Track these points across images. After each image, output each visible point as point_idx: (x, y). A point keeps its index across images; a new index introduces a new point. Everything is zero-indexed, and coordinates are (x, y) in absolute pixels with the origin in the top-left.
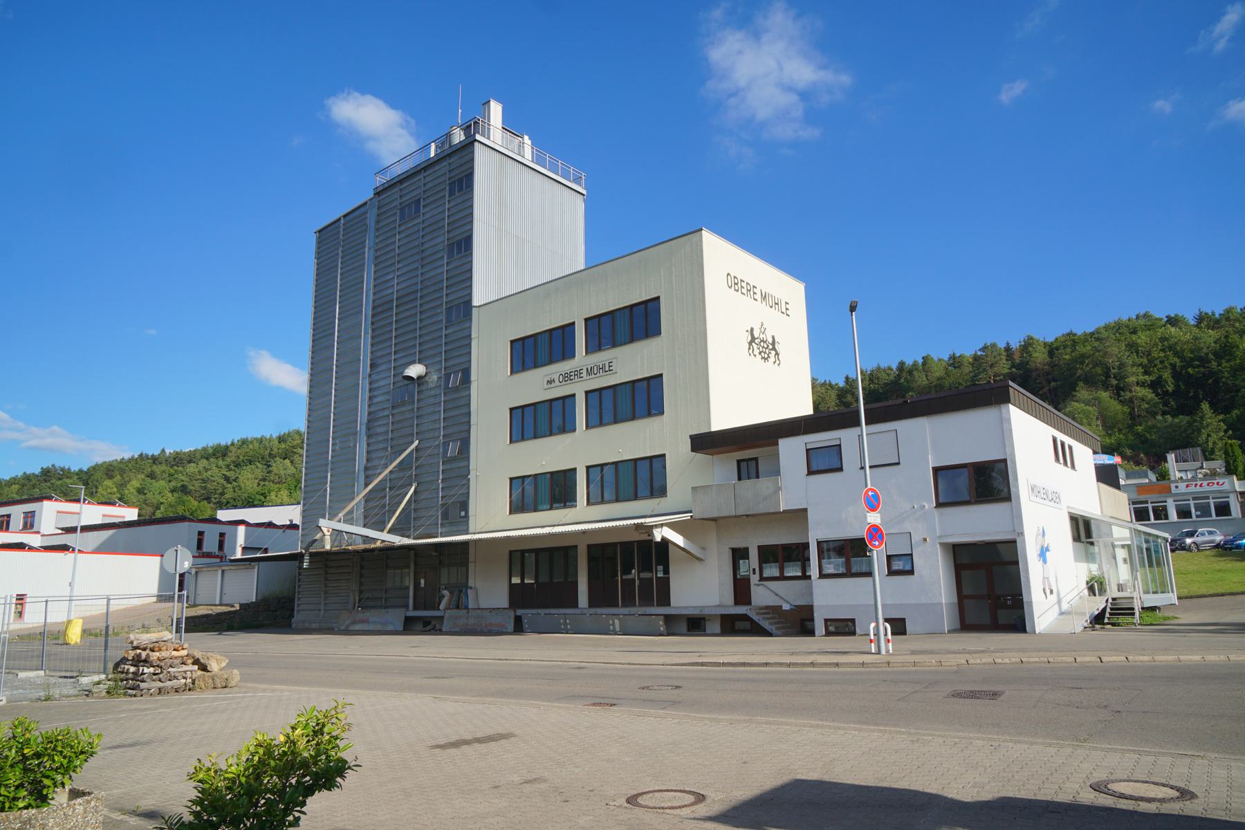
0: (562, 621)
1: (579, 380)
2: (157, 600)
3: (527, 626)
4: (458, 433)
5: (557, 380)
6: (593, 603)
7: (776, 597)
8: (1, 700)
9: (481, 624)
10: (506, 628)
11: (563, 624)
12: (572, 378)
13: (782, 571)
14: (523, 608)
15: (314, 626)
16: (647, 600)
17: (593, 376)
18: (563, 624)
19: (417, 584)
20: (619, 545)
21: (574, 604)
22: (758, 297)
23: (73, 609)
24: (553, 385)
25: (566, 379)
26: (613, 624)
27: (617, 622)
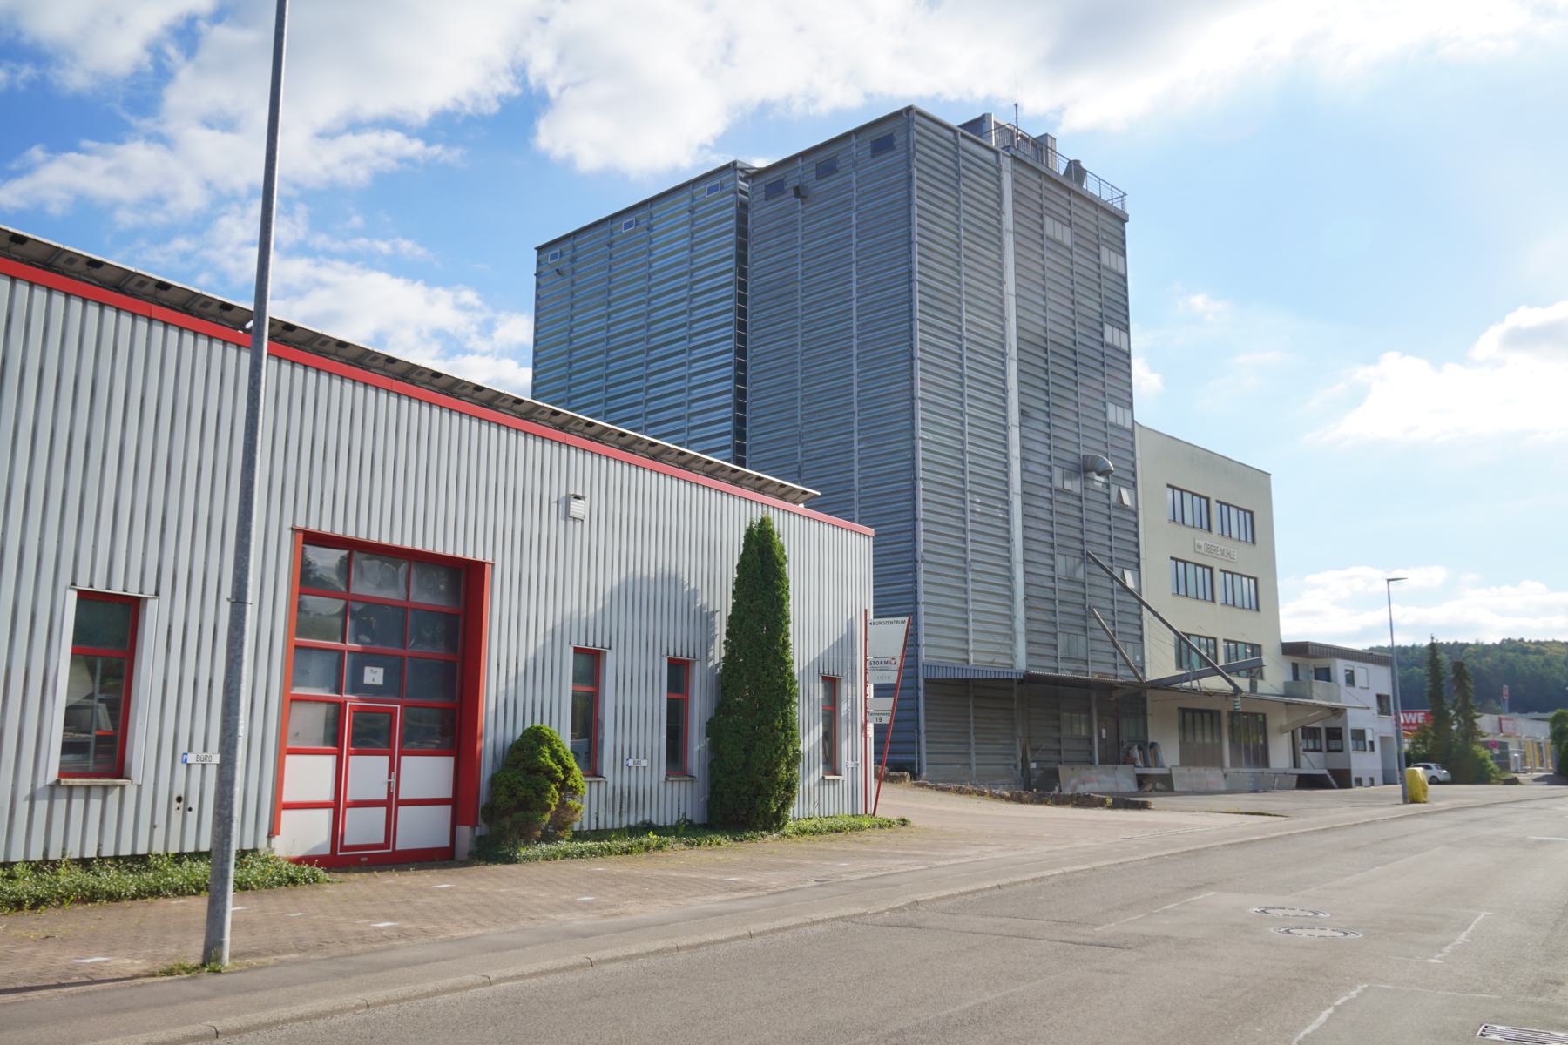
27: (1277, 780)
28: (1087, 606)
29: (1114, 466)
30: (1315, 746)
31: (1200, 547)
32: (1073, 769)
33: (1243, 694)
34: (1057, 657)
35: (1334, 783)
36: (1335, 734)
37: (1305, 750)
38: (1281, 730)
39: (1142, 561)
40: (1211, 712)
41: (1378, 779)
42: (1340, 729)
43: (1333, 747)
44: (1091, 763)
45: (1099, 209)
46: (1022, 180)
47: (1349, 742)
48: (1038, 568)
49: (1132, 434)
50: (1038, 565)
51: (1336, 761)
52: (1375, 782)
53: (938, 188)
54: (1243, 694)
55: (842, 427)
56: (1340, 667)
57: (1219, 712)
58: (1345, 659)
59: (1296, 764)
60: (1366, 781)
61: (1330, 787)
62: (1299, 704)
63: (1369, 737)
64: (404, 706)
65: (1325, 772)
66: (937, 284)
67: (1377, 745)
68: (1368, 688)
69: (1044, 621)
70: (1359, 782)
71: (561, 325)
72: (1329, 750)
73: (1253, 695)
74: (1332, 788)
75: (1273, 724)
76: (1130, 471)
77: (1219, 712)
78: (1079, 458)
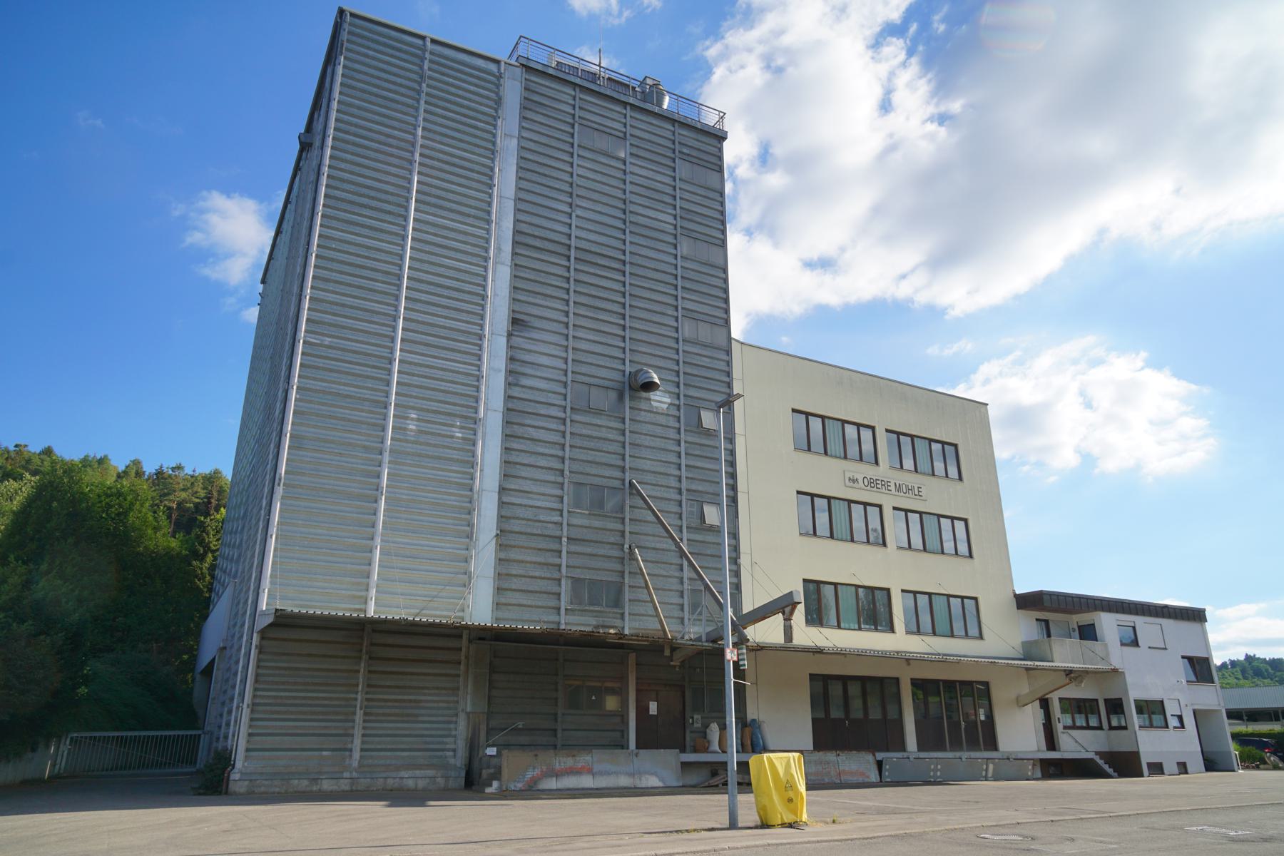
0: (932, 767)
1: (887, 492)
2: (1092, 713)
3: (887, 773)
4: (713, 494)
5: (860, 481)
6: (922, 746)
7: (1077, 745)
8: (886, 3)
9: (829, 772)
10: (868, 777)
11: (933, 770)
12: (878, 486)
13: (1074, 721)
14: (888, 750)
15: (327, 785)
16: (973, 744)
17: (902, 494)
18: (933, 770)
19: (642, 711)
20: (941, 683)
21: (902, 747)
22: (892, 488)
23: (346, 26)
24: (855, 485)
25: (872, 485)
26: (987, 770)
27: (991, 767)
28: (626, 546)
29: (659, 379)
30: (1119, 722)
31: (854, 481)
32: (536, 755)
33: (748, 644)
34: (559, 609)
35: (1110, 771)
36: (1116, 706)
37: (1065, 728)
38: (1020, 703)
39: (739, 495)
40: (881, 681)
41: (1196, 762)
42: (1121, 699)
43: (1115, 723)
44: (624, 746)
45: (676, 125)
46: (533, 86)
47: (1135, 719)
48: (532, 499)
49: (729, 352)
50: (531, 495)
51: (1119, 742)
52: (1189, 769)
53: (386, 81)
54: (748, 644)
55: (350, 377)
56: (1108, 623)
57: (896, 681)
58: (1117, 612)
59: (1051, 743)
60: (1170, 766)
61: (1104, 775)
62: (1044, 669)
63: (1171, 709)
64: (702, 718)
65: (1090, 755)
66: (370, 181)
67: (1189, 721)
68: (1165, 649)
69: (540, 564)
70: (1157, 768)
71: (334, 377)
72: (1111, 728)
73: (789, 645)
74: (1107, 776)
75: (1000, 695)
76: (673, 382)
77: (896, 681)
78: (624, 375)
